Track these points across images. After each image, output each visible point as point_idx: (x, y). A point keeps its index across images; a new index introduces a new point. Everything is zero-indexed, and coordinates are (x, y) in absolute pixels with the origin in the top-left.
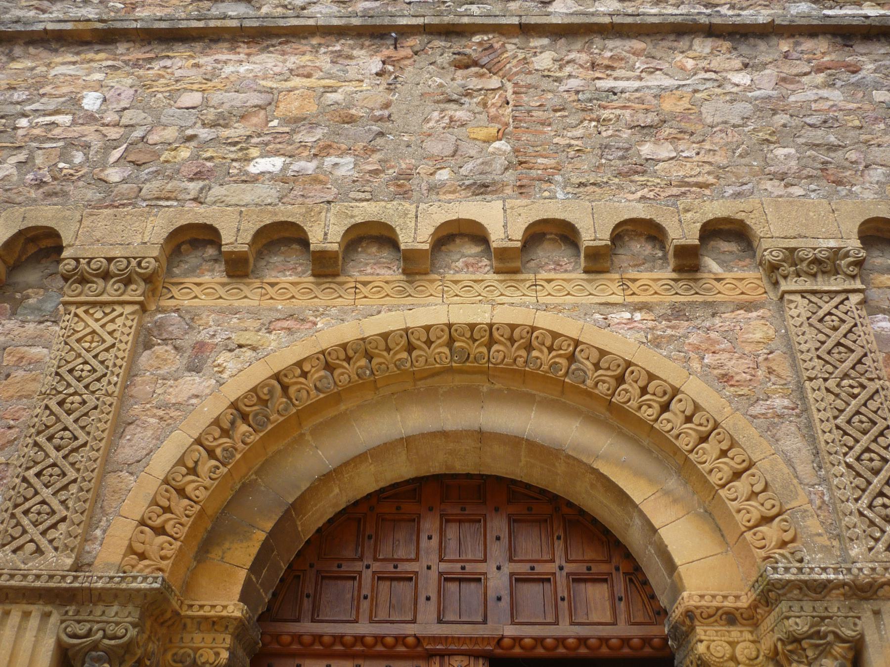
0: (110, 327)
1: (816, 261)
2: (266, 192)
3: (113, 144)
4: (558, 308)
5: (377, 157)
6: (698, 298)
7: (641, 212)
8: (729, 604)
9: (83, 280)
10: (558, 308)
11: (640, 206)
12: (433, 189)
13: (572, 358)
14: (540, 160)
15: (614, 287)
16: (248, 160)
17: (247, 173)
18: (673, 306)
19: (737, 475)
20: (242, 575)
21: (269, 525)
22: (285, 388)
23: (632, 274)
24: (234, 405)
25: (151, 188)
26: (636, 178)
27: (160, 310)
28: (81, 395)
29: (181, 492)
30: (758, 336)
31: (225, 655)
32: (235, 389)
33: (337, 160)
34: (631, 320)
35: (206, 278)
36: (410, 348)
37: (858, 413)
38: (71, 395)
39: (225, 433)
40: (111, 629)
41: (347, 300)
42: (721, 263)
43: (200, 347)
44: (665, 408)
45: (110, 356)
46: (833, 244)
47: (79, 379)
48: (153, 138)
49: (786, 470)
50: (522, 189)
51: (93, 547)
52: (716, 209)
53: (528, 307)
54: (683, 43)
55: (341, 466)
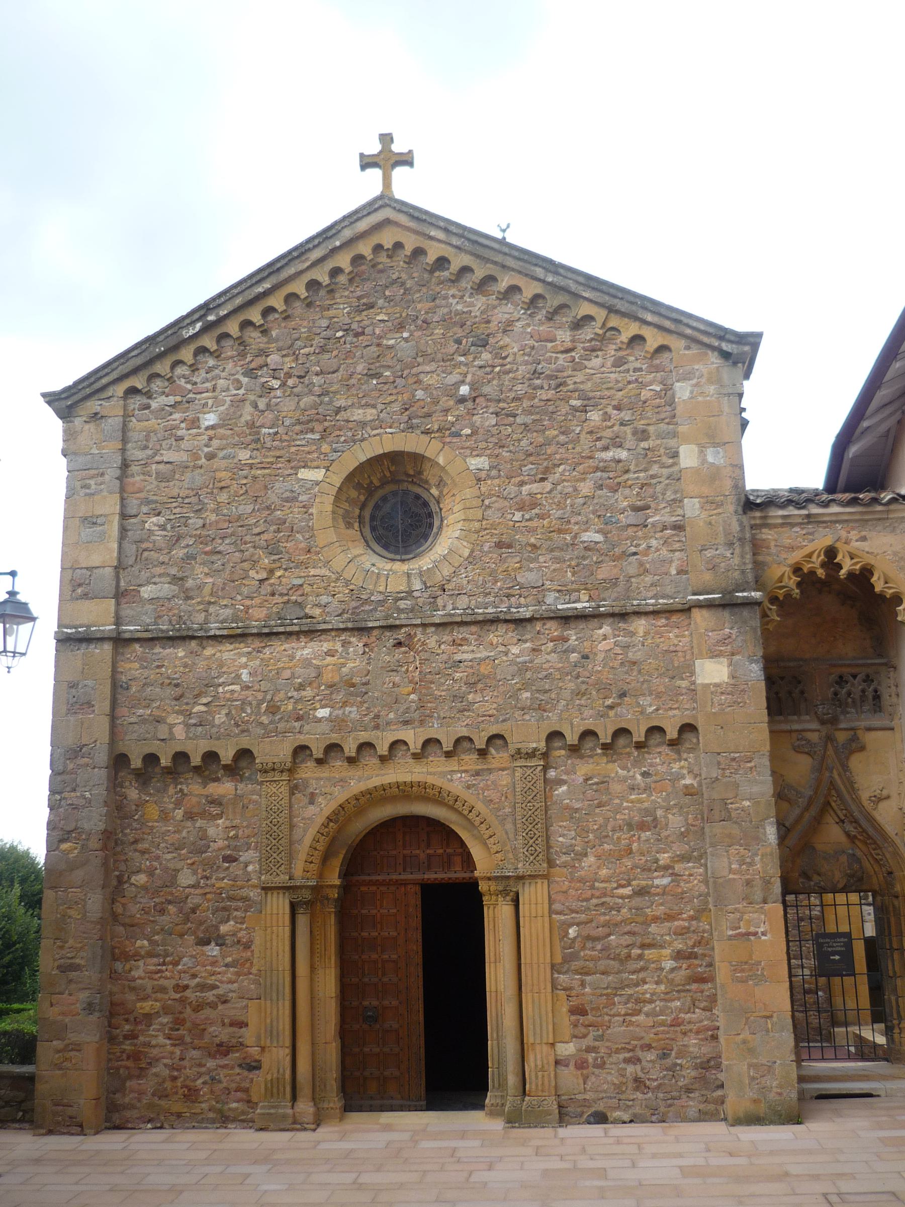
1: (527, 753)
2: (324, 727)
4: (434, 774)
5: (366, 705)
6: (485, 767)
8: (488, 875)
9: (266, 772)
10: (434, 774)
12: (388, 724)
13: (440, 792)
14: (429, 705)
15: (456, 763)
16: (315, 709)
17: (316, 717)
19: (491, 837)
20: (338, 870)
21: (344, 852)
22: (343, 808)
23: (463, 757)
24: (328, 818)
25: (281, 726)
26: (465, 713)
27: (295, 779)
29: (315, 849)
30: (505, 783)
31: (336, 895)
32: (327, 812)
33: (350, 709)
35: (309, 764)
36: (384, 790)
39: (326, 827)
41: (360, 773)
42: (495, 750)
43: (312, 794)
45: (282, 802)
48: (277, 699)
49: (505, 836)
51: (293, 870)
52: (494, 730)
54: (493, 628)
55: (341, 1027)
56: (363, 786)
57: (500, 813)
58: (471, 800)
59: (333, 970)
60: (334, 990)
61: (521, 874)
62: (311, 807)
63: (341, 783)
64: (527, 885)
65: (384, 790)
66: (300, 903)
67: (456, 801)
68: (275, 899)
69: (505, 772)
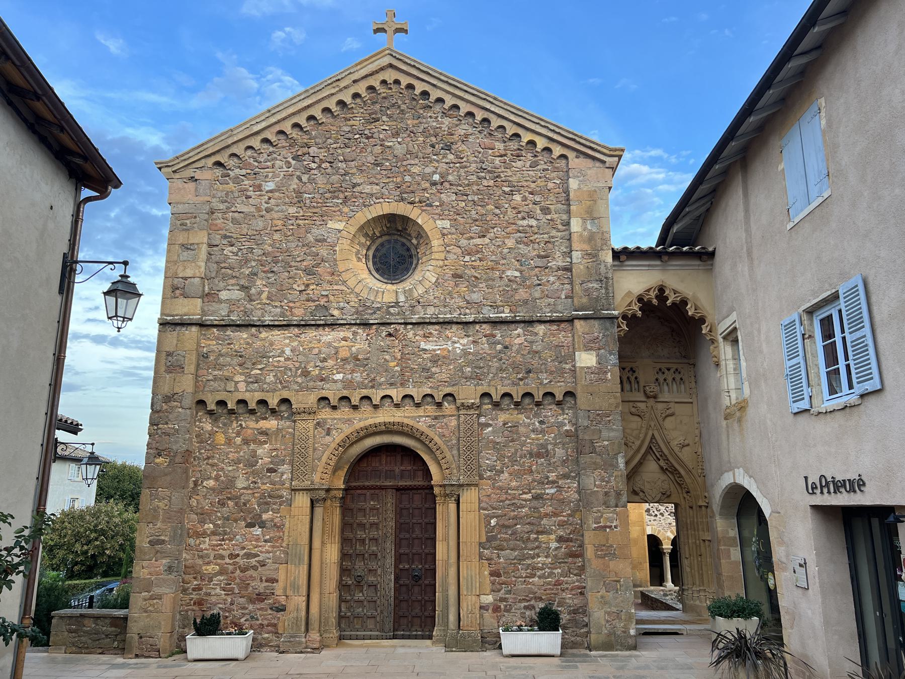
0: (307, 426)
3: (297, 369)
4: (408, 417)
7: (429, 391)
10: (408, 417)
11: (429, 390)
18: (435, 416)
19: (443, 458)
32: (338, 440)
34: (425, 420)
38: (225, 268)
40: (320, 495)
44: (430, 442)
46: (473, 401)
50: (402, 385)
59: (337, 544)
60: (336, 558)
61: (461, 483)
62: (327, 437)
63: (348, 422)
64: (465, 491)
65: (376, 427)
66: (318, 501)
69: (453, 418)
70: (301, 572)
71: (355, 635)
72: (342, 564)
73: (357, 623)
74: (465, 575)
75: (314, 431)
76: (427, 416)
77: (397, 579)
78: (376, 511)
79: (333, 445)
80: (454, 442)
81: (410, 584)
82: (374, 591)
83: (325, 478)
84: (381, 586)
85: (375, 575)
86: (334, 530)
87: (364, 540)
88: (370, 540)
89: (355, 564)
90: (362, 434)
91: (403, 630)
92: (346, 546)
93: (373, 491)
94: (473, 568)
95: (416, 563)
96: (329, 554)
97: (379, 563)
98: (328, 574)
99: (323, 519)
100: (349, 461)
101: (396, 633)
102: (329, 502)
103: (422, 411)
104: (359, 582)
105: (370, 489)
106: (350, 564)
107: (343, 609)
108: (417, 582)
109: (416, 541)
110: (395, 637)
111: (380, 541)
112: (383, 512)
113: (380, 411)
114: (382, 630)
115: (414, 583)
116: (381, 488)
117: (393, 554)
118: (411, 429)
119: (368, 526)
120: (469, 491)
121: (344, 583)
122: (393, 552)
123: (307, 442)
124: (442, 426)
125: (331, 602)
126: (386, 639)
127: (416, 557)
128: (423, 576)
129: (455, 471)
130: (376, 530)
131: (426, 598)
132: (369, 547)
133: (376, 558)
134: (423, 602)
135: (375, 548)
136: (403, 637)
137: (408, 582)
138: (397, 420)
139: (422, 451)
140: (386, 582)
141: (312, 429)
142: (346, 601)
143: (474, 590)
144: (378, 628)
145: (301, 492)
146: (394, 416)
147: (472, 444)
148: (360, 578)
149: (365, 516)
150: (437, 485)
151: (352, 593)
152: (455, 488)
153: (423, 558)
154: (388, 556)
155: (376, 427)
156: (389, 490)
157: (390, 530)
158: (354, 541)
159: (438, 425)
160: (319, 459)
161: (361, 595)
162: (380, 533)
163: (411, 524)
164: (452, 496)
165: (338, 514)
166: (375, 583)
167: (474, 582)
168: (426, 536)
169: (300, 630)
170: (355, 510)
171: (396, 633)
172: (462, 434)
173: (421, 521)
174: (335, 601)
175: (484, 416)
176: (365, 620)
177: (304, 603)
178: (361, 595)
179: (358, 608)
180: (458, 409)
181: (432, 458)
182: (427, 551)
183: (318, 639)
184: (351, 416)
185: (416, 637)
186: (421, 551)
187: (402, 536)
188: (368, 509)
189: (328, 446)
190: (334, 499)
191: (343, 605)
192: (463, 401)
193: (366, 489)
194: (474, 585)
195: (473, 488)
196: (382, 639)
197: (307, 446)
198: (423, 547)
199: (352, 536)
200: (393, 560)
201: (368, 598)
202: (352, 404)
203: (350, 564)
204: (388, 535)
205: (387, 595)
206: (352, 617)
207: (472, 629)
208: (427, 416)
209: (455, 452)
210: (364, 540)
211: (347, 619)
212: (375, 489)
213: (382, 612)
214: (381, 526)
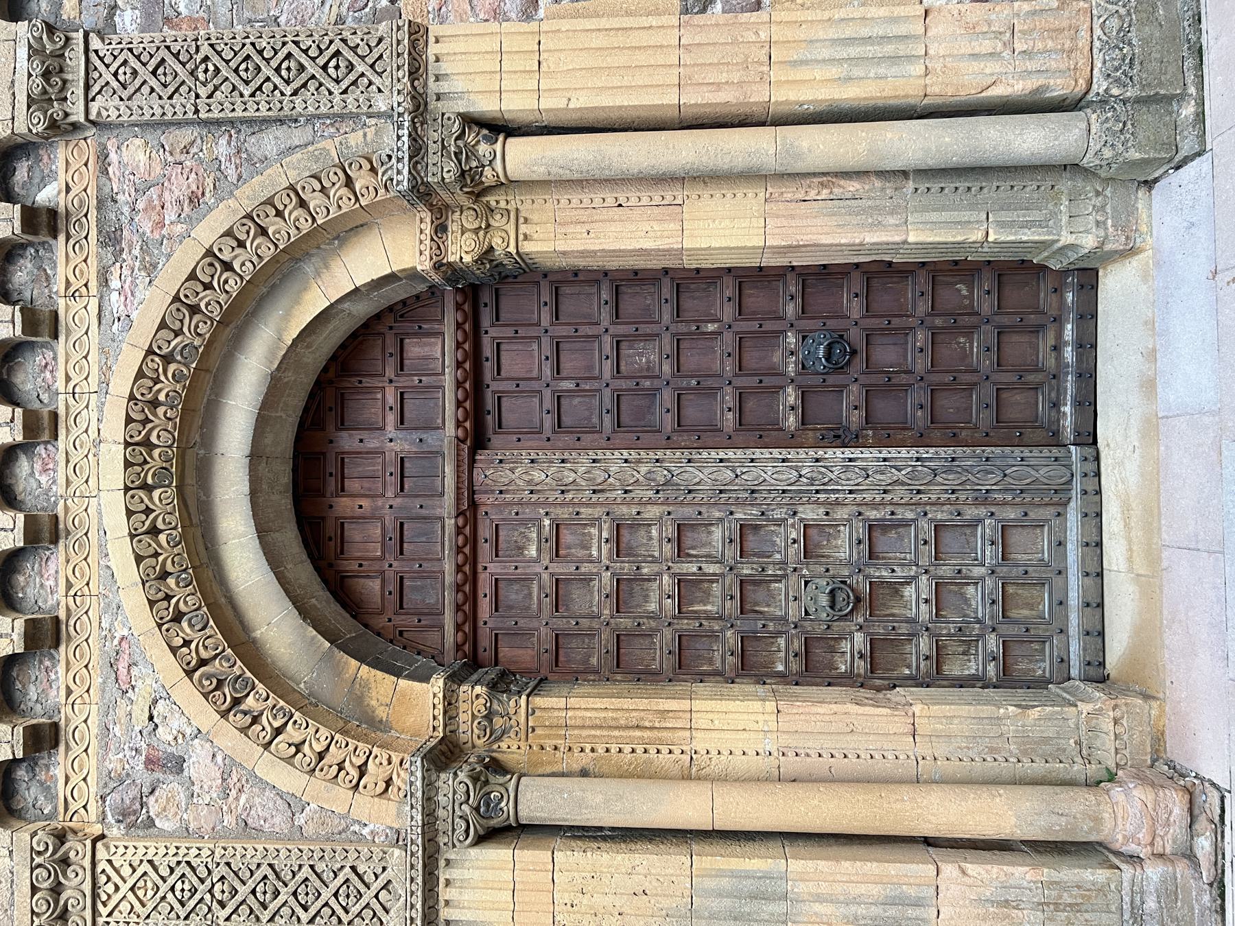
0: (126, 871)
1: (46, 75)
4: (106, 370)
10: (106, 370)
18: (103, 244)
19: (302, 204)
21: (354, 663)
28: (213, 885)
32: (204, 715)
37: (236, 71)
40: (461, 797)
42: (43, 184)
46: (23, 53)
47: (194, 891)
53: (103, 404)
56: (134, 600)
57: (232, 173)
58: (186, 258)
59: (697, 705)
60: (756, 705)
61: (408, 104)
62: (191, 769)
63: (122, 666)
64: (444, 87)
65: (154, 531)
66: (485, 808)
67: (194, 310)
68: (467, 896)
69: (113, 157)
70: (824, 888)
71: (1082, 616)
72: (783, 678)
73: (1031, 607)
74: (834, 71)
75: (163, 834)
76: (104, 282)
77: (840, 437)
78: (563, 531)
79: (228, 736)
80: (222, 148)
81: (863, 379)
82: (893, 534)
83: (383, 774)
84: (874, 505)
85: (827, 529)
86: (634, 717)
87: (681, 582)
88: (681, 553)
89: (784, 619)
90: (186, 598)
91: (1056, 405)
92: (711, 661)
93: (485, 549)
94: (802, 34)
95: (777, 357)
96: (739, 742)
97: (777, 514)
98: (828, 744)
99: (584, 773)
100: (326, 657)
101: (1068, 433)
102: (511, 750)
103: (76, 306)
104: (858, 600)
105: (474, 559)
106: (782, 641)
107: (972, 668)
108: (854, 352)
109: (691, 360)
110: (1087, 437)
111: (689, 512)
112: (572, 503)
113: (71, 511)
114: (1059, 498)
115: (859, 363)
116: (469, 510)
117: (740, 453)
118: (167, 359)
119: (627, 568)
120: (445, 67)
121: (861, 666)
122: (730, 454)
123: (202, 872)
124: (150, 207)
125: (954, 727)
126: (1098, 474)
127: (752, 358)
128: (831, 324)
129: (355, 139)
130: (642, 532)
131: (923, 307)
132: (710, 558)
133: (756, 528)
134: (938, 322)
135: (717, 533)
136: (1088, 404)
137: (854, 388)
138: (115, 429)
139: (287, 317)
140: (855, 478)
141: (152, 848)
142: (939, 656)
143: (902, 30)
144: (1049, 512)
145: (444, 894)
146: (98, 442)
147: (228, 55)
148: (841, 596)
149: (586, 580)
150: (439, 248)
151: (904, 629)
152: (432, 136)
153: (755, 326)
154: (751, 475)
155: (154, 531)
156: (478, 477)
157: (644, 469)
158: (685, 624)
159: (147, 227)
160: (293, 804)
161: (909, 592)
162: (652, 512)
163: (623, 384)
164: (472, 152)
165: (561, 702)
166: (860, 531)
167: (865, 32)
168: (666, 317)
169: (1102, 890)
170: (560, 624)
171: (1068, 433)
172: (182, 105)
173: (607, 339)
174: (947, 709)
175: (111, 15)
176: (1015, 572)
177: (970, 868)
178: (909, 592)
179: (966, 601)
180: (60, 129)
181: (318, 274)
182: (728, 312)
183: (1140, 794)
184: (95, 653)
185: (1087, 345)
186: (728, 336)
187: (669, 422)
188: (556, 568)
189: (231, 764)
190: (498, 722)
191: (954, 669)
192: (22, 99)
193: (474, 579)
194: (879, 31)
195: (433, 49)
196: (1099, 492)
197: (223, 870)
198: (711, 327)
199: (668, 633)
200: (766, 453)
201: (924, 561)
202: (20, 649)
203: (782, 641)
204: (661, 475)
205: (913, 475)
206: (1004, 629)
207: (1084, 33)
208: (104, 282)
209: (269, 142)
210: (681, 582)
211: (1016, 650)
212: (474, 541)
213: (983, 499)
214: (625, 509)
